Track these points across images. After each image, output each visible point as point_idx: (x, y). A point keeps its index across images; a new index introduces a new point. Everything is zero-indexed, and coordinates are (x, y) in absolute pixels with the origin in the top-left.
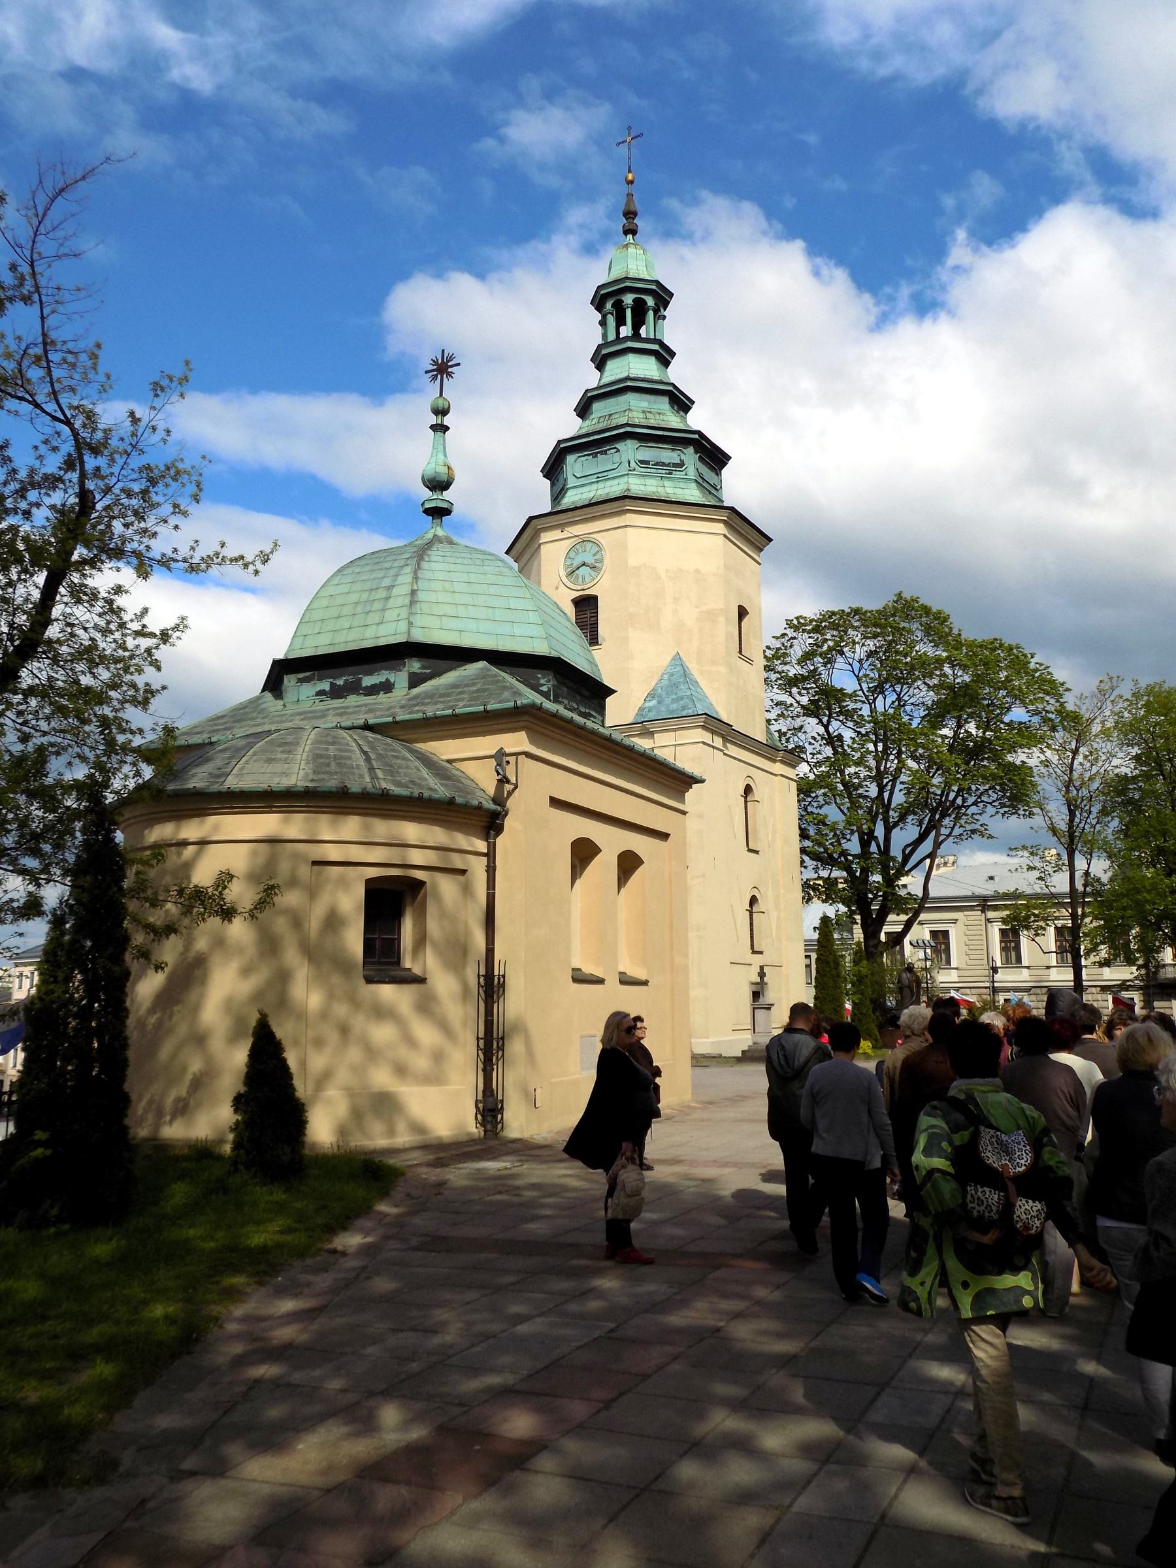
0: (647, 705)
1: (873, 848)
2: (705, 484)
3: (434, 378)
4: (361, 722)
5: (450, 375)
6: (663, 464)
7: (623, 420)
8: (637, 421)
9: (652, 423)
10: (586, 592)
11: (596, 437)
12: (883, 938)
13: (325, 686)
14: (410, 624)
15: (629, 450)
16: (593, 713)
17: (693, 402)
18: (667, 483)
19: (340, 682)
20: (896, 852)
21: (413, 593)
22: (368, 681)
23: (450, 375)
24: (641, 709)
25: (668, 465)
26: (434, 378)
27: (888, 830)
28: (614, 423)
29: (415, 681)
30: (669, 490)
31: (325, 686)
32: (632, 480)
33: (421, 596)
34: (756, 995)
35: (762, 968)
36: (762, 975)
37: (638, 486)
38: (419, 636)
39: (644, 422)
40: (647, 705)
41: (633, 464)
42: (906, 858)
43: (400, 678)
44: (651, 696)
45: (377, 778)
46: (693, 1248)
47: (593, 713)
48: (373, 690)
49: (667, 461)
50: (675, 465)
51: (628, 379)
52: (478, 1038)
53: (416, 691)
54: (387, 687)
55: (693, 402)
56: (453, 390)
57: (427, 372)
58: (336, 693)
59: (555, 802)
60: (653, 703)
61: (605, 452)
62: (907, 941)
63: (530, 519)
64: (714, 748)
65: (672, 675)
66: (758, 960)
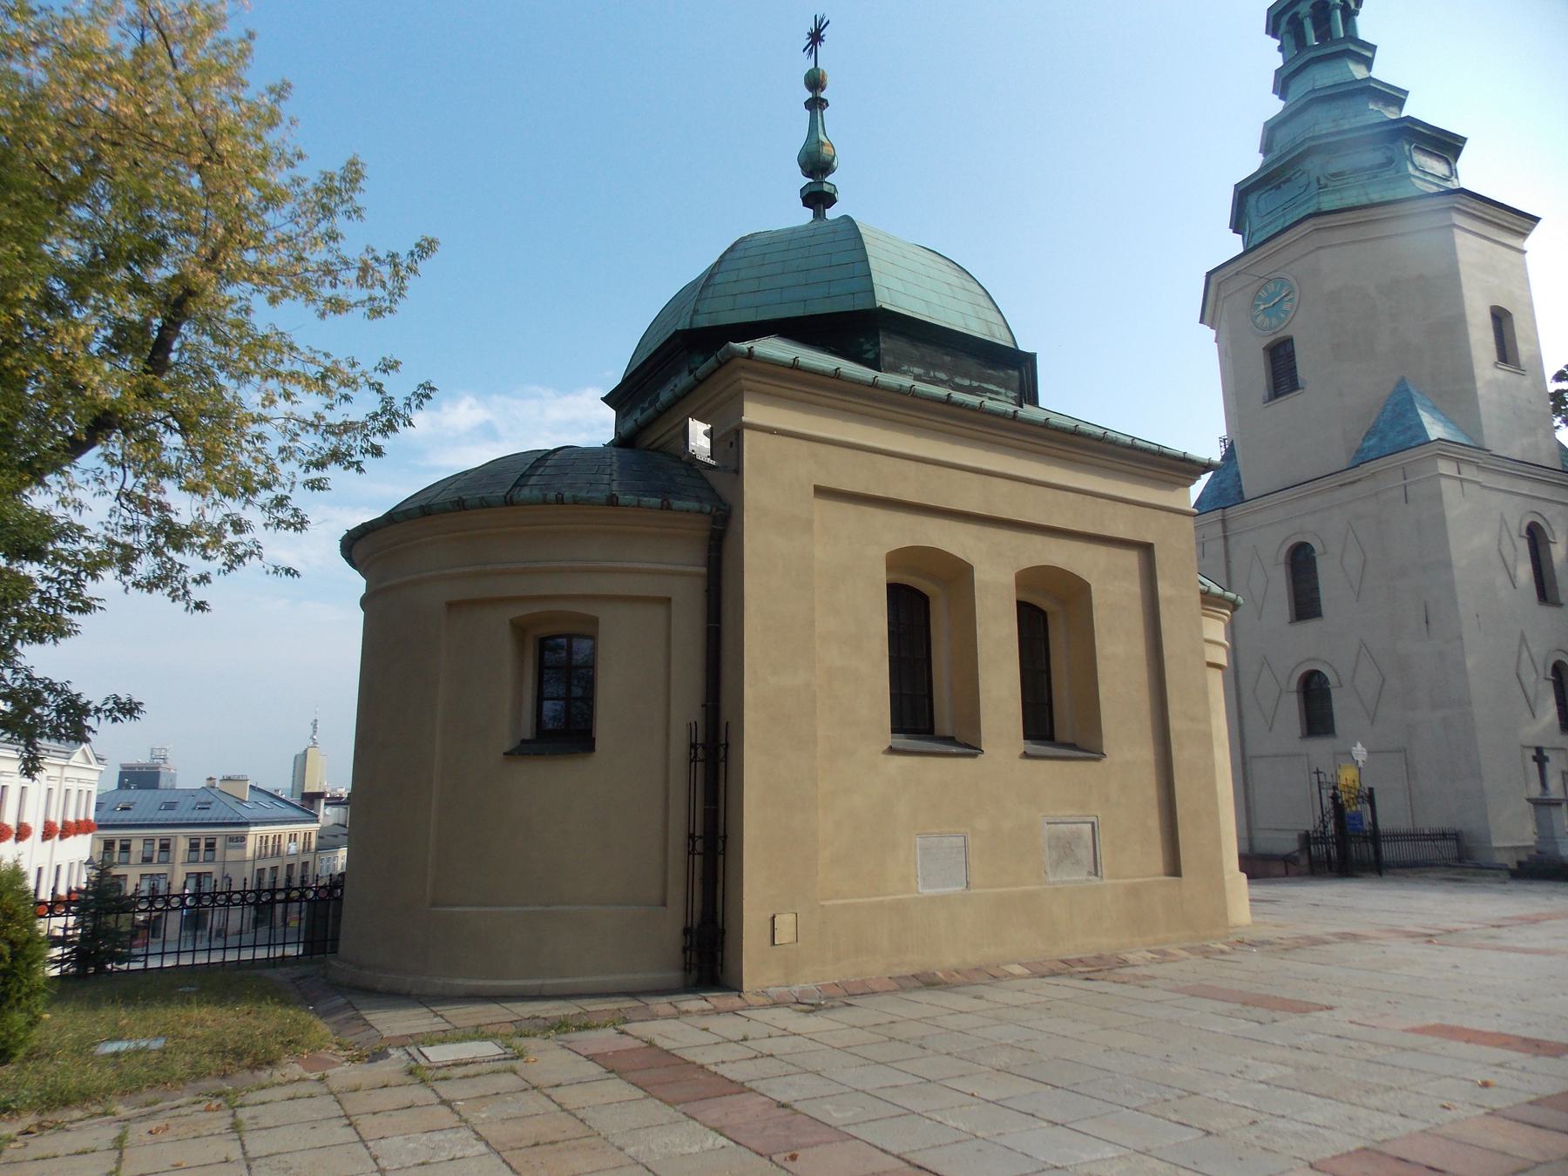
6: (1364, 169)
10: (1279, 335)
24: (1359, 451)
41: (1323, 181)
44: (1369, 434)
52: (691, 836)
59: (821, 492)
61: (1289, 180)
63: (1209, 274)
64: (1462, 480)
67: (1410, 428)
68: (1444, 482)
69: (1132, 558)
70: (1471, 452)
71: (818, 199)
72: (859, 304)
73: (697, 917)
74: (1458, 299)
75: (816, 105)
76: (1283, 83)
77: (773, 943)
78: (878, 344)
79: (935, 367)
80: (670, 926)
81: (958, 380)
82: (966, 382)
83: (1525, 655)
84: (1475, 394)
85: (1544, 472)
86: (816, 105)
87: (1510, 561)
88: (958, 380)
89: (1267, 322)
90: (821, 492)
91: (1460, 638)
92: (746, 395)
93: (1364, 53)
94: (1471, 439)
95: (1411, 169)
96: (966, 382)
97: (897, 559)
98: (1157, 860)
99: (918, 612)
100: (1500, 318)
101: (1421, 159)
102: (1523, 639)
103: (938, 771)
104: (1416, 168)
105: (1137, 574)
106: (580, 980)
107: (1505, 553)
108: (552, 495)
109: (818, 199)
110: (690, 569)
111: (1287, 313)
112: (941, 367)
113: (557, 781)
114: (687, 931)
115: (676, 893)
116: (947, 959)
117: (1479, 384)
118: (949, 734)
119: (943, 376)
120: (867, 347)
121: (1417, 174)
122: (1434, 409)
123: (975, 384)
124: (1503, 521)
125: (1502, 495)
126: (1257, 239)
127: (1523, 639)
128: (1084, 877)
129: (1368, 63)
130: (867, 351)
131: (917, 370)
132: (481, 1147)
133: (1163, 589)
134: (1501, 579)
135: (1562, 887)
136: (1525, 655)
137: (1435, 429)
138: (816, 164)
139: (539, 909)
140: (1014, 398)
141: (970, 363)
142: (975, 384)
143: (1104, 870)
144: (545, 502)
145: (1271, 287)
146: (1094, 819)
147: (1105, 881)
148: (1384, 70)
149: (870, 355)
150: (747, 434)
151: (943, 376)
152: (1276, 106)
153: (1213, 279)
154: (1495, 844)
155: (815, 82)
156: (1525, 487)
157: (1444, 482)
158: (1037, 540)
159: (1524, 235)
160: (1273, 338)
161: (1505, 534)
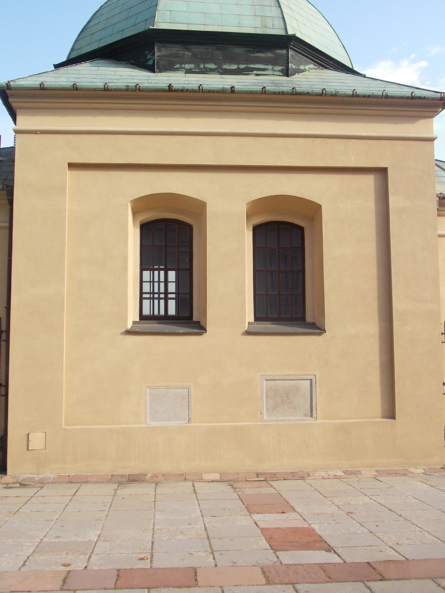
59: (72, 166)
77: (28, 449)
79: (205, 61)
81: (226, 67)
82: (234, 67)
88: (226, 67)
90: (72, 166)
96: (234, 67)
97: (257, 206)
99: (170, 239)
112: (211, 60)
119: (212, 66)
123: (242, 66)
131: (187, 66)
132: (377, 535)
133: (394, 201)
139: (252, 423)
140: (281, 71)
142: (242, 66)
146: (313, 378)
147: (319, 421)
149: (150, 63)
151: (212, 66)
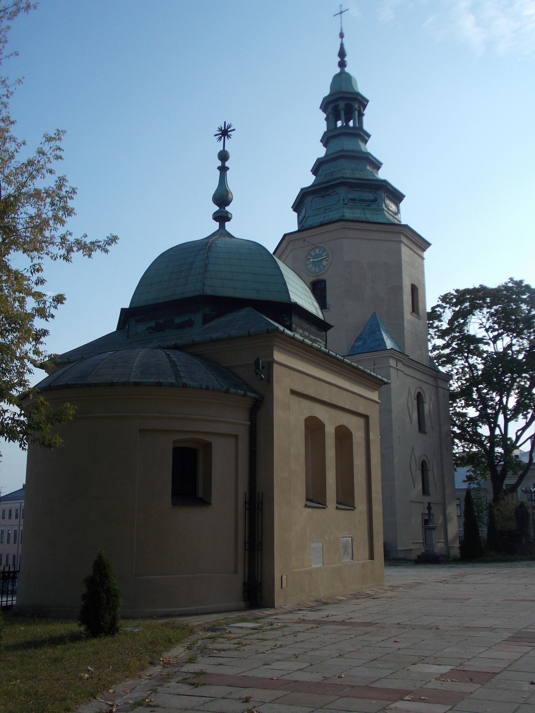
0: (357, 344)
1: (497, 432)
2: (390, 212)
3: (220, 139)
4: (173, 343)
5: (229, 136)
6: (364, 201)
7: (340, 175)
8: (348, 175)
9: (358, 176)
10: (319, 278)
11: (324, 185)
12: (504, 488)
13: (153, 324)
14: (204, 284)
15: (342, 192)
16: (319, 339)
17: (382, 164)
18: (367, 212)
19: (161, 321)
20: (512, 435)
21: (206, 265)
22: (178, 320)
23: (229, 136)
24: (353, 347)
25: (368, 201)
26: (220, 139)
27: (507, 421)
28: (334, 177)
29: (206, 320)
30: (368, 216)
31: (153, 324)
32: (346, 211)
33: (210, 267)
34: (426, 522)
35: (429, 504)
36: (429, 508)
37: (349, 214)
38: (209, 291)
39: (352, 176)
40: (357, 344)
41: (346, 201)
42: (518, 438)
43: (198, 318)
44: (359, 339)
45: (180, 377)
46: (377, 685)
47: (319, 339)
48: (181, 326)
49: (366, 198)
50: (372, 201)
51: (342, 151)
52: (245, 543)
53: (207, 325)
54: (189, 324)
55: (382, 164)
56: (231, 145)
57: (215, 135)
58: (159, 328)
59: (293, 392)
60: (360, 343)
61: (329, 195)
62: (519, 489)
63: (285, 236)
64: (398, 369)
65: (372, 326)
66: (427, 499)
67: (377, 340)
68: (391, 369)
69: (362, 421)
70: (400, 355)
71: (222, 217)
72: (283, 300)
73: (246, 578)
74: (401, 278)
75: (223, 169)
76: (326, 140)
78: (291, 319)
80: (238, 581)
83: (413, 457)
84: (403, 325)
85: (424, 368)
86: (223, 169)
87: (410, 409)
89: (313, 269)
90: (293, 392)
91: (392, 448)
92: (275, 347)
93: (365, 137)
94: (400, 348)
95: (384, 206)
98: (367, 555)
100: (414, 289)
101: (388, 202)
102: (413, 450)
103: (317, 514)
104: (386, 206)
105: (363, 429)
106: (172, 609)
107: (409, 406)
108: (204, 386)
109: (222, 217)
110: (243, 422)
111: (324, 266)
113: (190, 518)
114: (244, 584)
115: (240, 568)
116: (323, 594)
117: (405, 322)
118: (311, 498)
120: (286, 319)
121: (386, 209)
122: (387, 332)
124: (409, 392)
125: (410, 378)
126: (309, 222)
127: (413, 450)
128: (350, 560)
129: (366, 142)
130: (286, 321)
134: (408, 420)
135: (532, 559)
136: (413, 457)
137: (389, 344)
138: (222, 198)
141: (313, 329)
143: (355, 558)
144: (201, 388)
145: (317, 251)
146: (352, 536)
148: (372, 147)
149: (288, 323)
150: (275, 365)
152: (321, 152)
153: (287, 238)
154: (399, 549)
155: (223, 156)
156: (418, 375)
157: (391, 369)
158: (340, 413)
159: (424, 250)
160: (315, 278)
161: (410, 397)
